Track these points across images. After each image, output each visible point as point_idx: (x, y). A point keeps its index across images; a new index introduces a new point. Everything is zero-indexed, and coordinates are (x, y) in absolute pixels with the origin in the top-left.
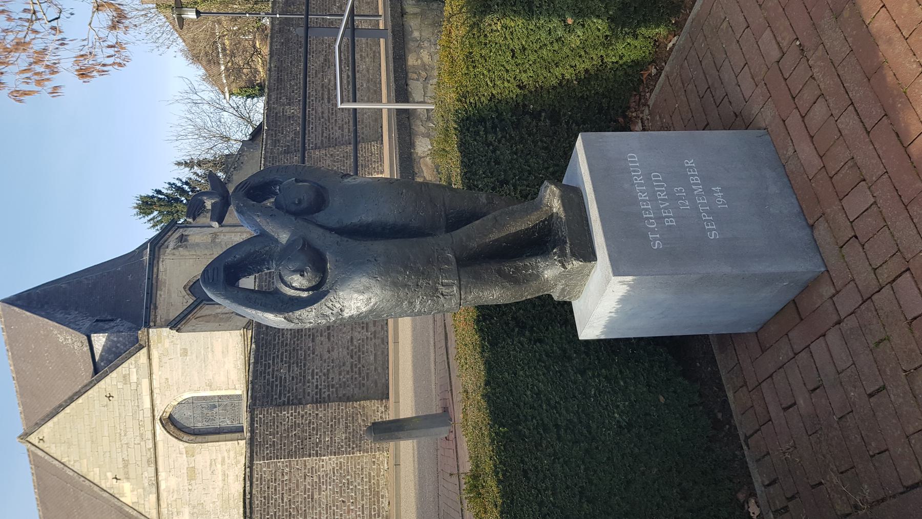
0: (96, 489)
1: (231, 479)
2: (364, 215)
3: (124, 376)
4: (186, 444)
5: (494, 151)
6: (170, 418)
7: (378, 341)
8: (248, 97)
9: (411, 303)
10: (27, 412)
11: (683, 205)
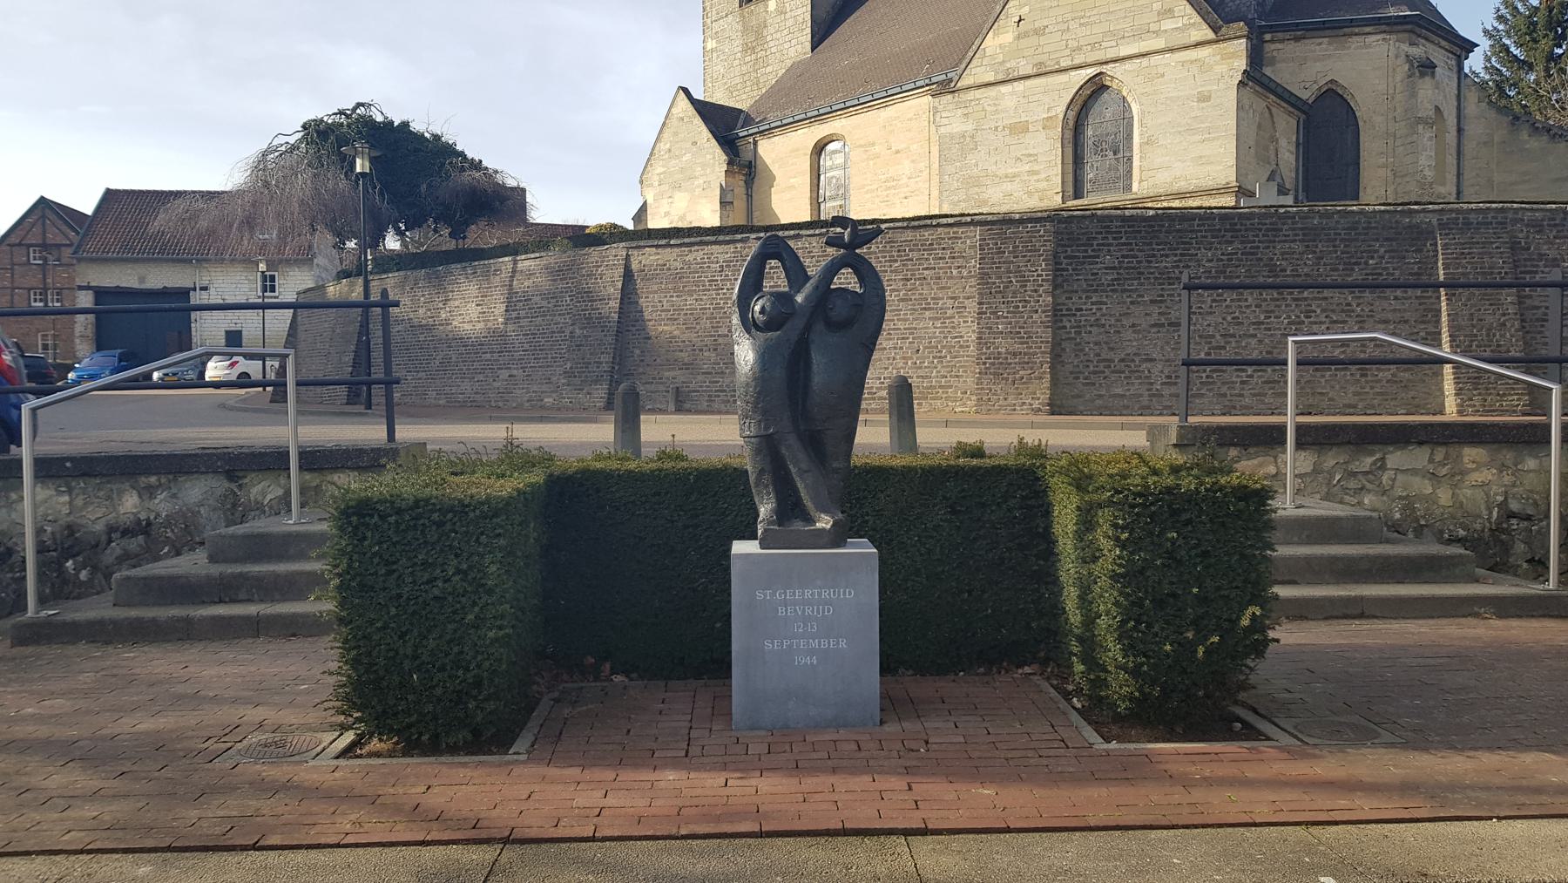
1: (1008, 187)
3: (1171, 10)
7: (1145, 400)
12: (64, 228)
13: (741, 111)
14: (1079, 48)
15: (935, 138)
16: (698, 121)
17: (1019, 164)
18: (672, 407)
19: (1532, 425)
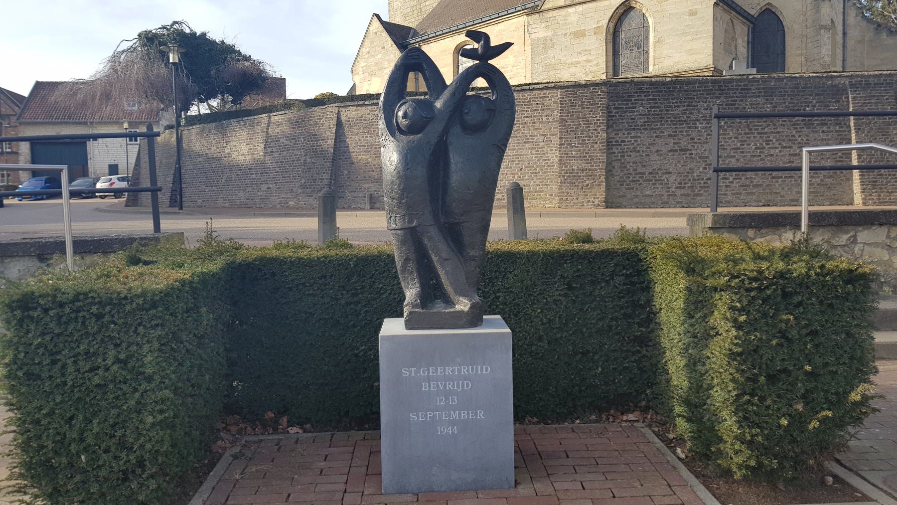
1: (573, 70)
4: (605, 26)
6: (631, 8)
12: (11, 105)
13: (411, 28)
15: (528, 42)
16: (385, 34)
18: (368, 206)
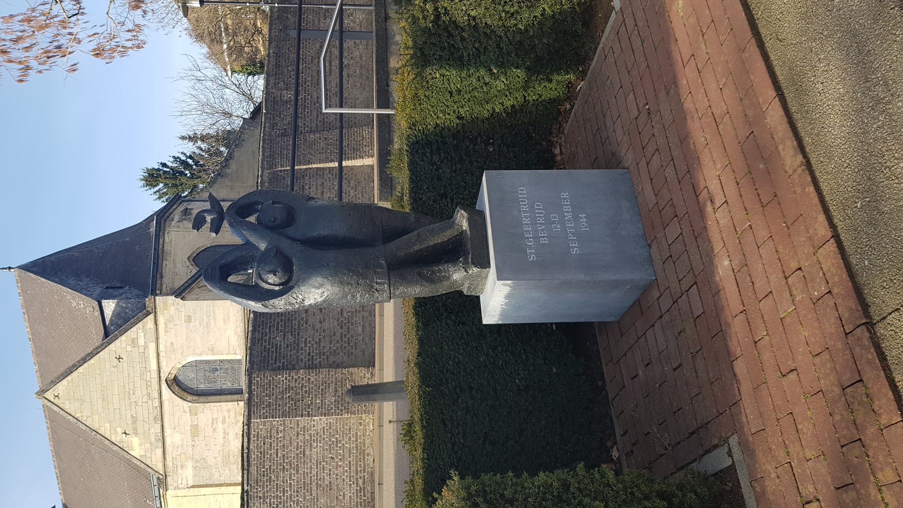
0: (107, 442)
1: (231, 436)
2: (323, 230)
4: (190, 404)
5: (437, 170)
7: (366, 314)
8: (249, 74)
9: (353, 296)
10: (42, 372)
11: (556, 227)
14: (149, 394)
17: (217, 430)
19: (378, 123)
